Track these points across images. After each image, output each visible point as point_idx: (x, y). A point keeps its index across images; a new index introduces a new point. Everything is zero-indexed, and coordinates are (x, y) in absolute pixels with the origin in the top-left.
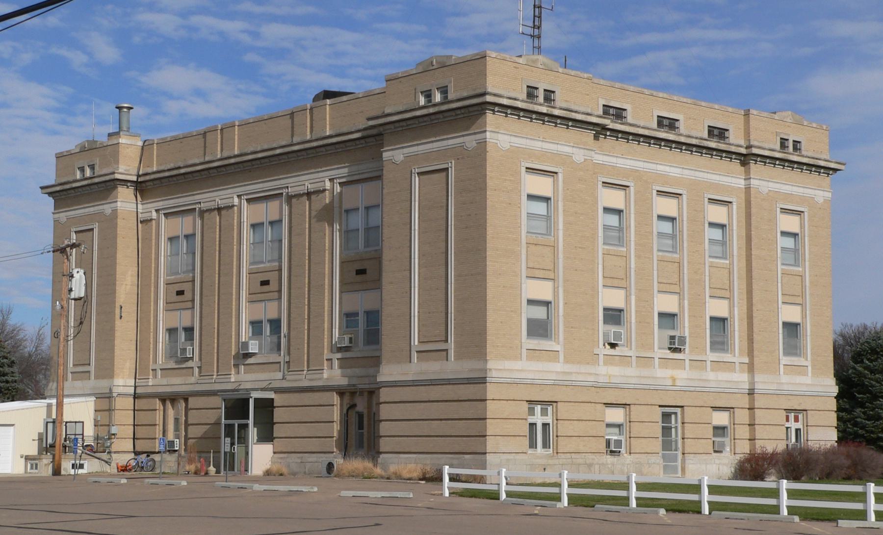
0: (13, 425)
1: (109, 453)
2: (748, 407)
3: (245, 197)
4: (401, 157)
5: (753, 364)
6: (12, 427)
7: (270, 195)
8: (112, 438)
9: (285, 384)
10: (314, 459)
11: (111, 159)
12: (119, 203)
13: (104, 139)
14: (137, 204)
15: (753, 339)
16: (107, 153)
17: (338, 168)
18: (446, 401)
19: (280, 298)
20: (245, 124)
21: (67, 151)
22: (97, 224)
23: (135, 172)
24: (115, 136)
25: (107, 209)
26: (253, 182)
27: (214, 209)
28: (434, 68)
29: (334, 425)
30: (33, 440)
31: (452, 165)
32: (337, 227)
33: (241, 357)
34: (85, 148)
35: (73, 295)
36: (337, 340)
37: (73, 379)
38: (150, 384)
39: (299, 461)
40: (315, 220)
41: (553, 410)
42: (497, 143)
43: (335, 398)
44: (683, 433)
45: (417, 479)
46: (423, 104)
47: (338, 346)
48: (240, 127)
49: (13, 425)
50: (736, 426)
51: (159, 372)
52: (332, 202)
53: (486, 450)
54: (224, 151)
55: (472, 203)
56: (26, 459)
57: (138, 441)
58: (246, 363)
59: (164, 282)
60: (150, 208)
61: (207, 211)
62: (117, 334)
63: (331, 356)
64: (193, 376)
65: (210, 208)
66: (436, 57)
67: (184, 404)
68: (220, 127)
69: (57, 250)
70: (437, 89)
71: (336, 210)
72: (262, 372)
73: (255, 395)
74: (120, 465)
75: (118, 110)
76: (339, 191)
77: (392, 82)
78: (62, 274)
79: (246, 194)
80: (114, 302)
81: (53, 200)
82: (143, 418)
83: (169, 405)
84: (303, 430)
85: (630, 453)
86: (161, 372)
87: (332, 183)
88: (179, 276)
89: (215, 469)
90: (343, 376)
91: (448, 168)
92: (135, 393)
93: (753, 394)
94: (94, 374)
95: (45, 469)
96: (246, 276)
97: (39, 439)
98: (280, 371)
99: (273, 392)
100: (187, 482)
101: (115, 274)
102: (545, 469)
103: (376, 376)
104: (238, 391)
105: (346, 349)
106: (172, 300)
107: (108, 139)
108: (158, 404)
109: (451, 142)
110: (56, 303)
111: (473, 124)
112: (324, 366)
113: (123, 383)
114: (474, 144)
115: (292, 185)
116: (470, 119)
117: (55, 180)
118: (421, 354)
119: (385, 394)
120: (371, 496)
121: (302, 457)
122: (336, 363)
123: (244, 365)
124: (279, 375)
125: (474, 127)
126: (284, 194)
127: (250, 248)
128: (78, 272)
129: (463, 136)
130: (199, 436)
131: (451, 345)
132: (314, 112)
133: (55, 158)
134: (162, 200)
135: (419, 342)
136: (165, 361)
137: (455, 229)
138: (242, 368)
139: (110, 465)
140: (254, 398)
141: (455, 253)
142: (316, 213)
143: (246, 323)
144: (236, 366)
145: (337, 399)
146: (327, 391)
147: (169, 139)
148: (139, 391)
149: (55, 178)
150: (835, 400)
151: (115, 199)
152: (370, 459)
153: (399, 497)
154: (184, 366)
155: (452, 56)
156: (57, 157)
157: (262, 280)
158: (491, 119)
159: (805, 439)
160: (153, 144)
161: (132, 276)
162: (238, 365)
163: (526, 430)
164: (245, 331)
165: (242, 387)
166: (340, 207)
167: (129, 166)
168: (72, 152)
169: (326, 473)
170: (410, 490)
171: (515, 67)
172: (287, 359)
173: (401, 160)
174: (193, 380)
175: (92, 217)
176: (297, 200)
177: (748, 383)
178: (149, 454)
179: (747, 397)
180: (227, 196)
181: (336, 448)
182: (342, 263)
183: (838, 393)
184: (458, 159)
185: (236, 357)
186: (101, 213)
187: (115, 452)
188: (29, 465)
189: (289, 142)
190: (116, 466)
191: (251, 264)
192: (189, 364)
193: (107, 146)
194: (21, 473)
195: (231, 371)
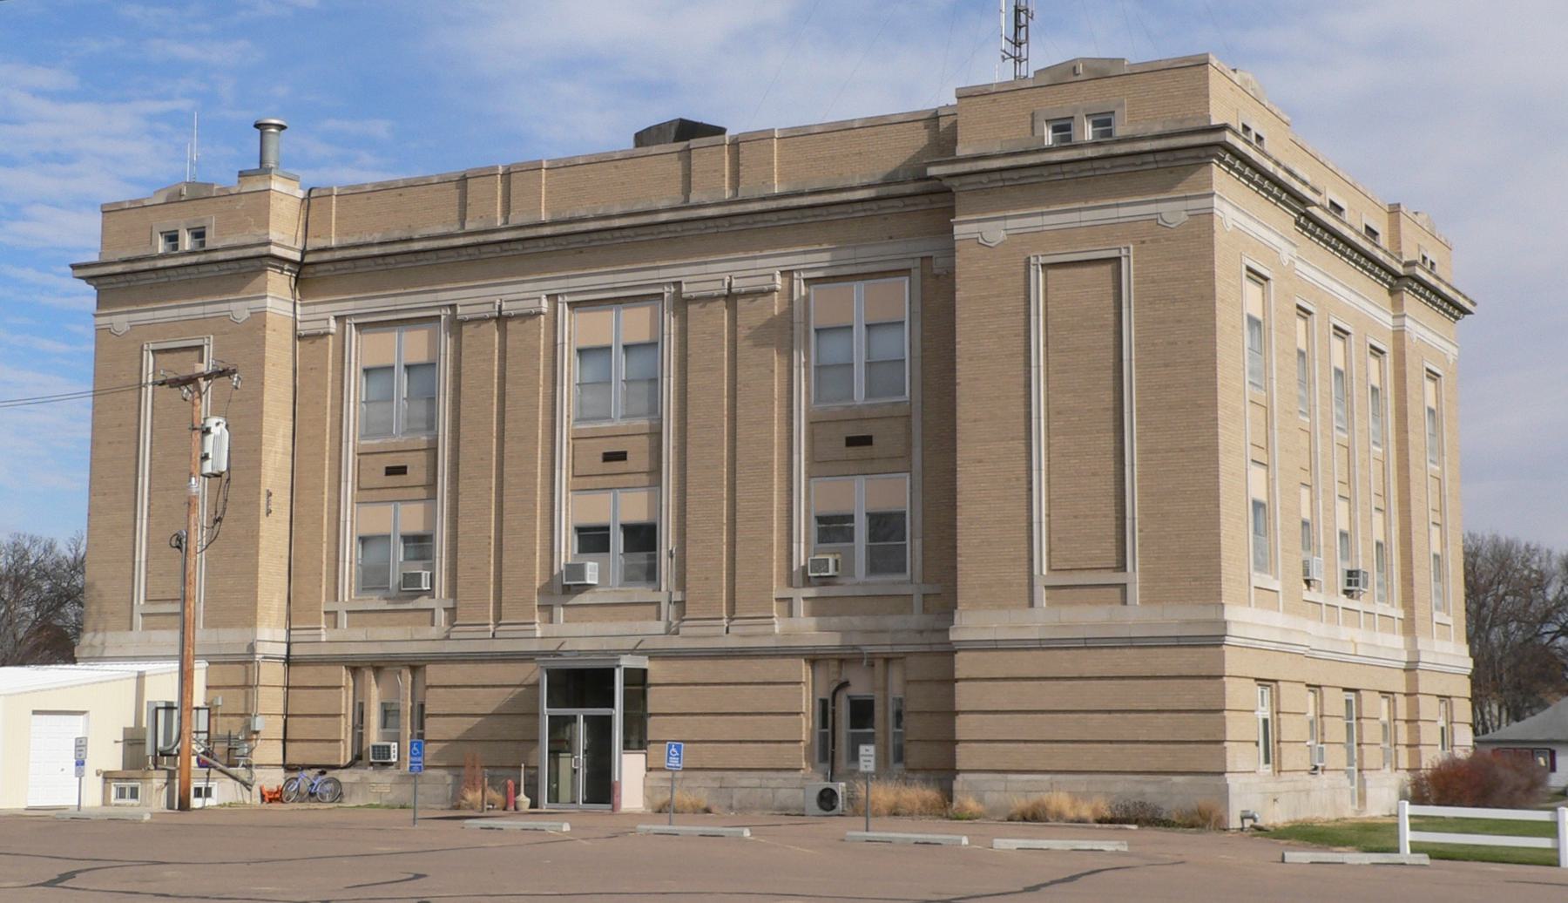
0: (83, 713)
1: (248, 766)
2: (1404, 691)
3: (567, 299)
4: (1002, 235)
5: (1413, 620)
6: (81, 717)
7: (648, 295)
8: (251, 740)
9: (677, 643)
10: (756, 782)
11: (249, 218)
12: (269, 300)
13: (230, 181)
14: (295, 304)
15: (1412, 579)
16: (238, 207)
17: (805, 253)
18: (1123, 678)
19: (432, 497)
20: (565, 167)
21: (131, 201)
22: (212, 337)
23: (300, 246)
24: (258, 177)
25: (240, 310)
26: (514, 279)
27: (490, 319)
28: (1079, 78)
29: (801, 720)
30: (116, 742)
31: (1129, 252)
32: (799, 357)
33: (558, 590)
34: (181, 195)
35: (208, 467)
36: (563, 568)
37: (146, 627)
38: (324, 639)
39: (716, 785)
40: (750, 343)
41: (1271, 695)
42: (977, 238)
43: (804, 670)
44: (1360, 736)
45: (1091, 819)
46: (1090, 138)
47: (565, 583)
48: (550, 172)
49: (83, 713)
50: (1324, 718)
51: (344, 619)
52: (790, 310)
53: (1225, 766)
54: (512, 214)
55: (1179, 321)
56: (105, 778)
57: (293, 744)
58: (570, 602)
59: (354, 450)
60: (323, 313)
61: (471, 321)
62: (263, 543)
63: (789, 593)
64: (433, 625)
65: (481, 315)
66: (1083, 60)
67: (410, 676)
68: (501, 171)
69: (163, 383)
70: (1087, 116)
71: (798, 330)
72: (611, 621)
73: (627, 662)
74: (266, 789)
75: (258, 131)
76: (803, 293)
77: (974, 100)
78: (190, 426)
79: (569, 294)
80: (258, 485)
82: (303, 701)
83: (369, 676)
84: (722, 728)
85: (1279, 771)
87: (787, 279)
88: (390, 440)
89: (528, 800)
90: (820, 629)
91: (1119, 259)
92: (288, 654)
93: (1414, 670)
94: (204, 619)
95: (153, 796)
96: (568, 443)
97: (124, 741)
98: (659, 619)
99: (646, 657)
100: (571, 827)
101: (260, 432)
102: (1275, 800)
103: (948, 630)
104: (560, 655)
105: (826, 581)
106: (376, 484)
107: (239, 182)
108: (345, 677)
109: (1124, 211)
110: (190, 481)
111: (1180, 181)
112: (772, 612)
113: (270, 636)
114: (1184, 217)
115: (510, 297)
118: (1053, 591)
119: (964, 664)
120: (1349, 861)
121: (722, 778)
122: (800, 607)
123: (563, 606)
124: (660, 627)
125: (1180, 187)
126: (443, 317)
127: (362, 409)
128: (218, 424)
129: (1157, 201)
130: (454, 736)
131: (1134, 576)
132: (741, 150)
134: (355, 299)
135: (1050, 568)
136: (356, 595)
137: (1137, 367)
138: (560, 613)
139: (250, 790)
140: (625, 669)
141: (1138, 410)
142: (749, 331)
143: (567, 529)
144: (547, 608)
145: (807, 672)
146: (784, 656)
147: (369, 188)
148: (295, 651)
150: (1469, 681)
151: (260, 291)
153: (1407, 862)
154: (410, 606)
155: (1123, 59)
156: (103, 212)
157: (607, 451)
158: (1220, 177)
159: (1276, 739)
160: (331, 195)
161: (284, 436)
162: (551, 606)
163: (654, 728)
164: (567, 547)
165: (567, 647)
166: (807, 324)
167: (283, 233)
169: (817, 808)
171: (1231, 89)
172: (677, 597)
173: (1001, 240)
174: (433, 632)
175: (199, 324)
176: (701, 307)
177: (1405, 652)
178: (324, 769)
179: (1403, 675)
180: (527, 295)
181: (807, 762)
182: (813, 424)
183: (1473, 670)
184: (1143, 242)
185: (546, 590)
186: (227, 318)
187: (259, 766)
188: (113, 790)
189: (679, 202)
190: (259, 791)
191: (578, 420)
192: (424, 602)
193: (239, 194)
194: (96, 808)
195: (534, 617)
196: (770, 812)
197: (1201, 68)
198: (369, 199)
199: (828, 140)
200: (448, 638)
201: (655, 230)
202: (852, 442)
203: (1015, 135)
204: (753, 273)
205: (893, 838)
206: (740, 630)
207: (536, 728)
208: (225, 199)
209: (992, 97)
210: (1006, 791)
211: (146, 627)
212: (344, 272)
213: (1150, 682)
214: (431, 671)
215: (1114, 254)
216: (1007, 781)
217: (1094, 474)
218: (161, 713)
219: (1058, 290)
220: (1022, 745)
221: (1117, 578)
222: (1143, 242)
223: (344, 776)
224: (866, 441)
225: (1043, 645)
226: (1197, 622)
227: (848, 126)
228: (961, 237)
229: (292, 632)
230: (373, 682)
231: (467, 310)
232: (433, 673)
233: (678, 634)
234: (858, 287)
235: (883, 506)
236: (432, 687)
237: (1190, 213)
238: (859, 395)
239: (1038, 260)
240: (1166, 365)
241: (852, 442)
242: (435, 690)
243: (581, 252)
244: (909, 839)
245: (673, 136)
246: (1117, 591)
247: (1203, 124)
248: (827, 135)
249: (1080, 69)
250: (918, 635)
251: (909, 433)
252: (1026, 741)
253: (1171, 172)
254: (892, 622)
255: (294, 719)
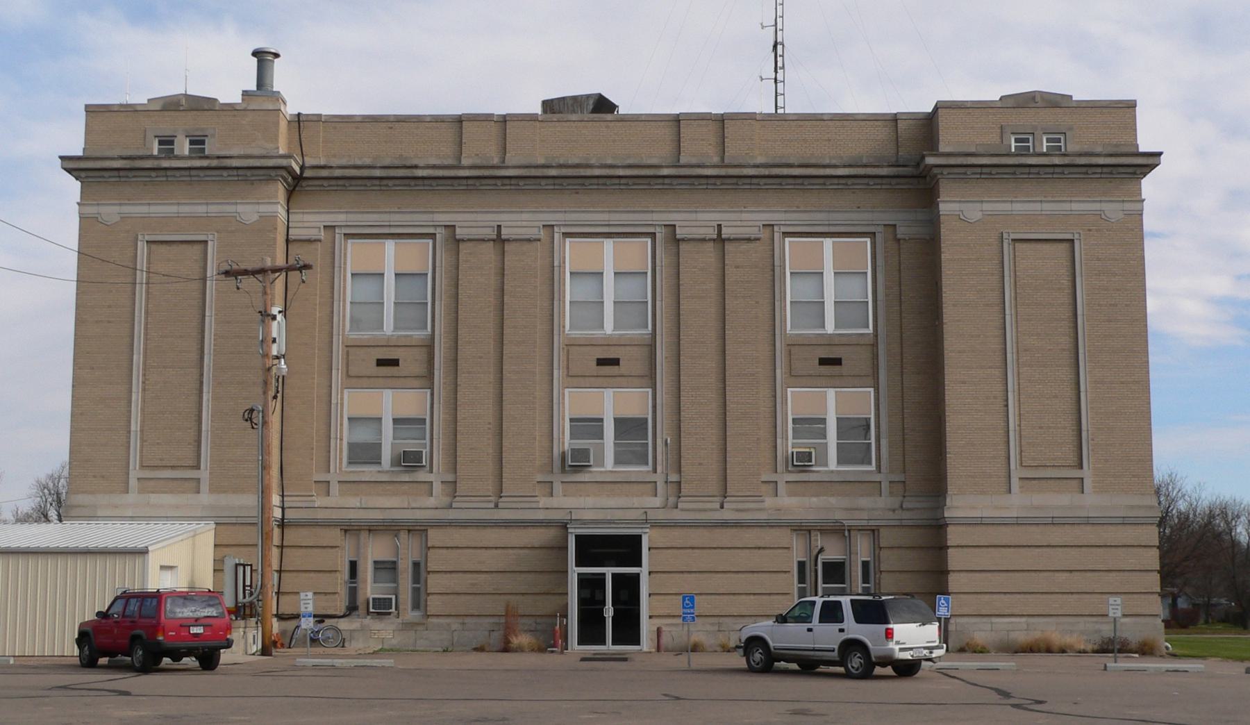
4: (979, 215)
16: (244, 122)
28: (1038, 105)
42: (97, 218)
51: (335, 488)
81: (80, 183)
86: (339, 486)
92: (283, 519)
98: (656, 496)
116: (253, 184)
117: (84, 149)
124: (657, 501)
133: (85, 113)
148: (290, 515)
149: (83, 146)
152: (162, 625)
168: (238, 108)
170: (1202, 664)
172: (674, 477)
173: (255, 219)
174: (431, 502)
184: (1090, 230)
192: (422, 476)
196: (675, 653)
197: (1130, 110)
198: (357, 128)
199: (801, 126)
200: (450, 507)
201: (456, 182)
202: (824, 362)
203: (992, 138)
204: (739, 223)
205: (1148, 667)
206: (734, 506)
207: (565, 583)
208: (229, 113)
209: (967, 111)
210: (992, 630)
211: (142, 491)
212: (335, 188)
213: (1101, 550)
214: (435, 536)
215: (1069, 236)
216: (992, 623)
217: (1056, 397)
218: (241, 569)
219: (1023, 259)
220: (1002, 596)
221: (1076, 473)
222: (1090, 230)
223: (343, 624)
224: (837, 362)
225: (1018, 522)
226: (1139, 507)
227: (819, 117)
228: (945, 213)
229: (285, 499)
230: (371, 546)
231: (465, 231)
232: (435, 536)
233: (677, 508)
234: (608, 244)
235: (854, 413)
236: (433, 547)
237: (1125, 212)
238: (609, 327)
239: (1009, 236)
240: (1109, 321)
241: (824, 362)
242: (437, 550)
243: (577, 193)
244: (1161, 668)
245: (591, 107)
246: (1075, 483)
247: (1133, 150)
248: (801, 123)
249: (1038, 99)
250: (891, 513)
251: (875, 357)
252: (1005, 593)
253: (1110, 182)
254: (864, 502)
255: (956, 574)
